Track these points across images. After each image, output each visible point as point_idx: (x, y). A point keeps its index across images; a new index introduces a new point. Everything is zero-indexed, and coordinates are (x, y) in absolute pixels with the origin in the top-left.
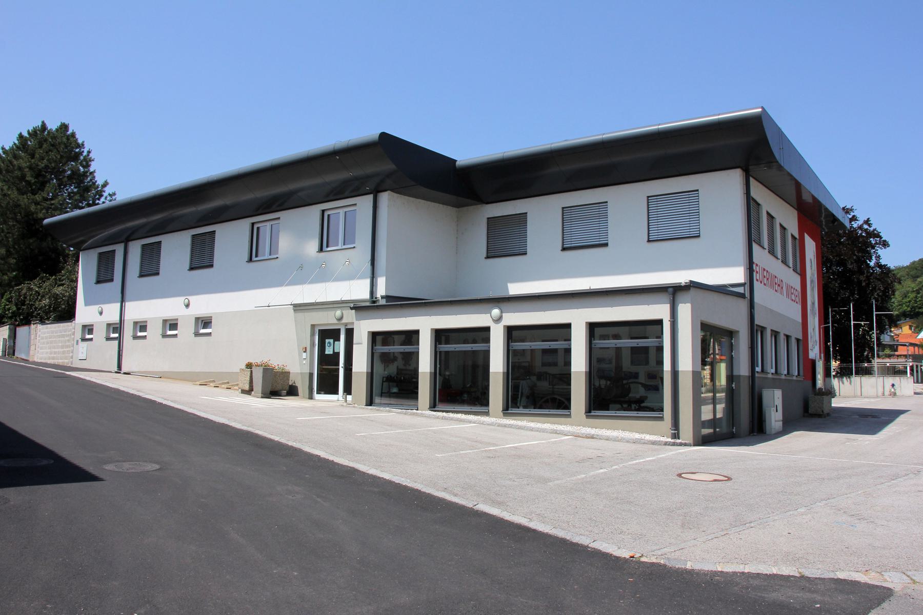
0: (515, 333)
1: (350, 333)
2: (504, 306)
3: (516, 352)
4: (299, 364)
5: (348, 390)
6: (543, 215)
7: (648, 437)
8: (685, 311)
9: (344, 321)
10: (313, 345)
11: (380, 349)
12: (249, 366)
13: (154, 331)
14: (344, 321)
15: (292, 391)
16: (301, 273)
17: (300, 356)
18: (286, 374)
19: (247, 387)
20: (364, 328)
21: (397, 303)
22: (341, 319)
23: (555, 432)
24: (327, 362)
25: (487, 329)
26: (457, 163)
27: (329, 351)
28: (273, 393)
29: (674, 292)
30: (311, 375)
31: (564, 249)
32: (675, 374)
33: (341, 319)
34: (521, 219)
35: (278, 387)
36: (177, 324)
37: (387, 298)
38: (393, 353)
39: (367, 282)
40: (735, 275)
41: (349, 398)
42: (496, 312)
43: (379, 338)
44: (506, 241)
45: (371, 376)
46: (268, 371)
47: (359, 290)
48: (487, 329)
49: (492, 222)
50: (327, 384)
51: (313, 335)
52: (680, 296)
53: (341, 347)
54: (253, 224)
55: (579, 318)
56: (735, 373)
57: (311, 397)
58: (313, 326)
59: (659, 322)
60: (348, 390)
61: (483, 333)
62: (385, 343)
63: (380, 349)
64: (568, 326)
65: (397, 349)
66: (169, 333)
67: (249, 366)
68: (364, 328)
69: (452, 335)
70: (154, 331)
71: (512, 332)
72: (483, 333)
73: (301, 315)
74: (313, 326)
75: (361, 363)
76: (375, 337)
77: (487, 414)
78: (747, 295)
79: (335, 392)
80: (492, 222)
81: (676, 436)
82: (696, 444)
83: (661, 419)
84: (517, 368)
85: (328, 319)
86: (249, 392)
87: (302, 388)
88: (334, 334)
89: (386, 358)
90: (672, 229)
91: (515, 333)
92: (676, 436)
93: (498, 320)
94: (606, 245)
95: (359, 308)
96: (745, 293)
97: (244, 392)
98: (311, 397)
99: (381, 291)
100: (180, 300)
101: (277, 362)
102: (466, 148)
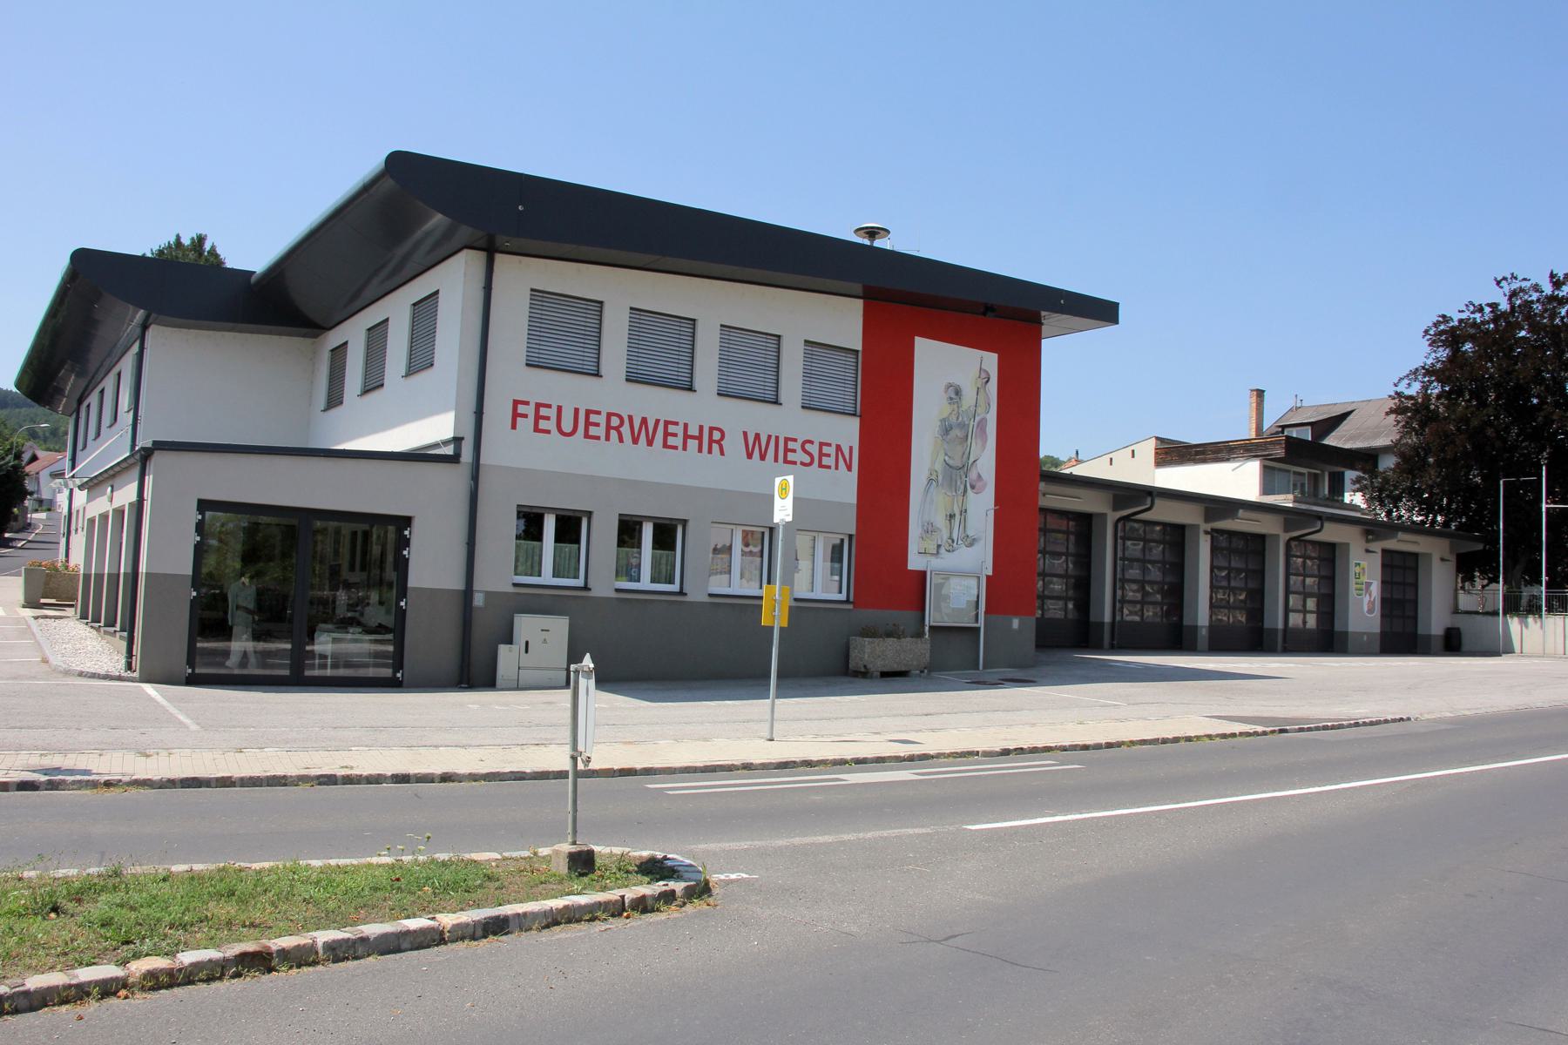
78: (467, 455)
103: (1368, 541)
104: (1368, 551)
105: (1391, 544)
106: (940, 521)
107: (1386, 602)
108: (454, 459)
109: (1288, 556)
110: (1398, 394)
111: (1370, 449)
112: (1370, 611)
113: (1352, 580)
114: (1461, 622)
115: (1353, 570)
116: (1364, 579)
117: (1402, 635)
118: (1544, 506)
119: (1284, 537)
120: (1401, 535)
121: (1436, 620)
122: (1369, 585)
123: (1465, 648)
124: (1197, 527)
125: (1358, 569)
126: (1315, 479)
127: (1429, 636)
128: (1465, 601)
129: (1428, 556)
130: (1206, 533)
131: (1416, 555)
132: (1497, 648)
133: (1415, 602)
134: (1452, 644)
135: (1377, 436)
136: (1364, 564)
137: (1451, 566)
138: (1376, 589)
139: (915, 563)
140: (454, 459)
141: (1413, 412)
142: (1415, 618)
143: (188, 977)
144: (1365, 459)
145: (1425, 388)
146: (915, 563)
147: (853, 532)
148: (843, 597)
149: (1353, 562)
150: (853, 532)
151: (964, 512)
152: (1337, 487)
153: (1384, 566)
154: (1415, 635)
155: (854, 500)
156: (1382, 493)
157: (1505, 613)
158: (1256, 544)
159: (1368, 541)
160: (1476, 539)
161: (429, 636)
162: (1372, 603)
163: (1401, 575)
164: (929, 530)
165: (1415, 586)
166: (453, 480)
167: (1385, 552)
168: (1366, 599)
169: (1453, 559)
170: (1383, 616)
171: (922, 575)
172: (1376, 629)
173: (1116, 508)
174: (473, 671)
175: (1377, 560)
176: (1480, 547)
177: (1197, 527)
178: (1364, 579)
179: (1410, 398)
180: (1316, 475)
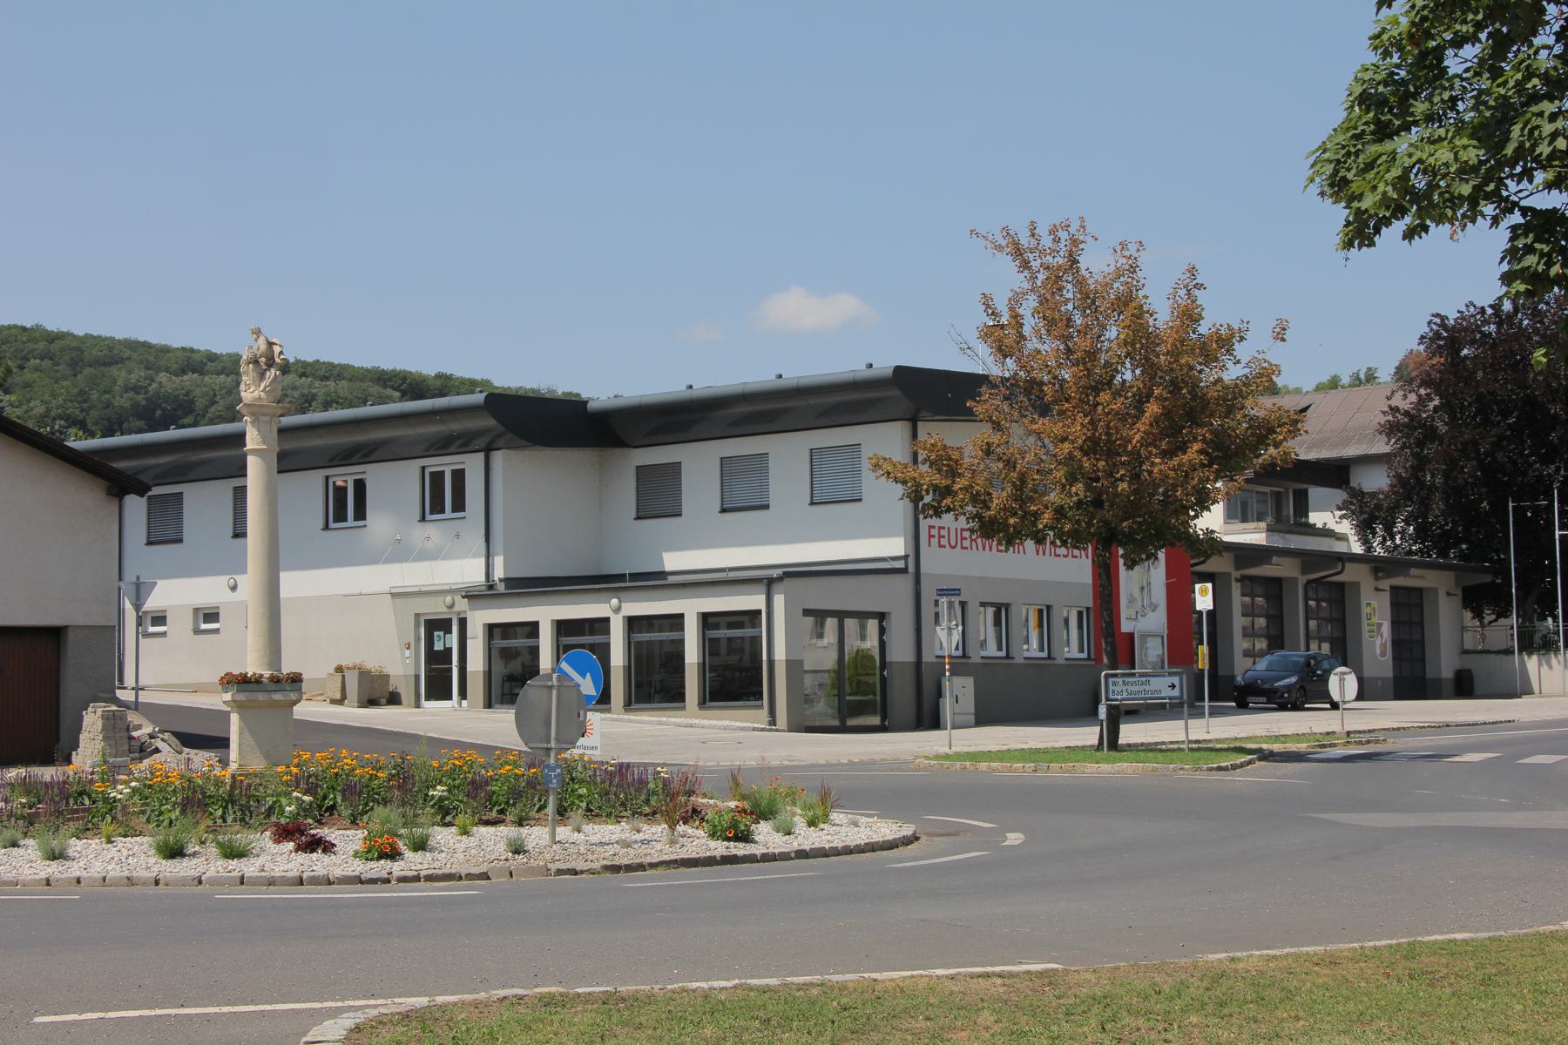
0: (710, 620)
1: (463, 623)
2: (623, 595)
3: (639, 643)
4: (401, 663)
5: (463, 694)
6: (700, 464)
7: (738, 724)
8: (779, 601)
9: (456, 609)
10: (418, 639)
11: (499, 643)
12: (339, 669)
13: (180, 626)
14: (456, 609)
15: (394, 699)
16: (400, 553)
17: (403, 654)
18: (385, 678)
19: (338, 696)
20: (479, 619)
21: (523, 587)
22: (452, 606)
23: (661, 723)
24: (437, 661)
25: (607, 620)
26: (591, 405)
27: (438, 646)
28: (372, 702)
29: (767, 580)
30: (417, 677)
31: (723, 511)
32: (771, 663)
33: (452, 606)
34: (675, 469)
35: (376, 695)
36: (217, 614)
37: (507, 581)
38: (514, 647)
39: (483, 561)
40: (893, 546)
41: (464, 703)
42: (615, 601)
43: (497, 631)
44: (659, 497)
45: (488, 675)
46: (365, 675)
47: (470, 571)
48: (607, 620)
49: (642, 471)
50: (438, 687)
51: (417, 626)
52: (776, 587)
53: (453, 640)
54: (327, 478)
55: (691, 607)
56: (888, 659)
57: (418, 706)
58: (417, 616)
59: (759, 612)
60: (463, 694)
61: (676, 621)
62: (505, 636)
63: (499, 643)
64: (681, 616)
65: (520, 642)
66: (204, 626)
67: (339, 669)
68: (479, 619)
69: (656, 622)
70: (180, 626)
71: (707, 620)
72: (676, 621)
73: (399, 601)
74: (417, 616)
75: (476, 661)
76: (491, 629)
77: (609, 710)
78: (911, 569)
79: (450, 698)
80: (642, 471)
81: (773, 722)
82: (790, 730)
83: (761, 707)
84: (640, 658)
85: (437, 609)
86: (340, 702)
87: (406, 694)
88: (443, 625)
89: (507, 654)
90: (831, 492)
91: (710, 620)
92: (773, 722)
93: (617, 610)
94: (767, 507)
95: (474, 596)
96: (909, 568)
97: (333, 702)
98: (418, 706)
99: (499, 573)
100: (223, 581)
101: (372, 664)
102: (605, 384)
103: (1377, 578)
104: (1377, 589)
105: (1400, 581)
106: (1137, 593)
107: (1397, 643)
108: (904, 571)
109: (1306, 599)
110: (1394, 410)
111: (1336, 460)
112: (1383, 654)
113: (1365, 622)
114: (1472, 663)
115: (1366, 610)
116: (1375, 620)
117: (1412, 681)
118: (1557, 533)
119: (1302, 580)
120: (1413, 571)
121: (1446, 664)
122: (1380, 625)
123: (1477, 692)
124: (1229, 574)
125: (1369, 610)
126: (1278, 498)
127: (1440, 680)
128: (1470, 641)
129: (1435, 590)
130: (1237, 580)
131: (1420, 590)
132: (1516, 689)
133: (1422, 642)
134: (1464, 687)
135: (1347, 441)
136: (1374, 603)
137: (1457, 601)
138: (1386, 629)
139: (1126, 627)
140: (904, 571)
141: (1403, 426)
142: (1423, 660)
143: (1225, 769)
144: (1335, 473)
145: (1422, 401)
146: (1126, 627)
147: (1091, 605)
148: (1085, 655)
149: (1364, 602)
150: (1091, 605)
151: (1149, 584)
152: (1302, 507)
153: (1392, 604)
154: (1424, 678)
155: (1090, 581)
156: (1369, 515)
157: (1520, 652)
158: (1275, 589)
159: (1377, 578)
160: (1486, 571)
161: (902, 695)
162: (1383, 645)
163: (1409, 612)
164: (1132, 601)
165: (1421, 624)
166: (904, 584)
167: (1394, 589)
168: (1378, 642)
169: (1459, 592)
170: (1394, 659)
171: (1131, 636)
172: (1389, 673)
173: (1304, 572)
174: (928, 718)
175: (1386, 598)
176: (1488, 578)
177: (1229, 574)
178: (1375, 620)
179: (1406, 413)
180: (1278, 494)
